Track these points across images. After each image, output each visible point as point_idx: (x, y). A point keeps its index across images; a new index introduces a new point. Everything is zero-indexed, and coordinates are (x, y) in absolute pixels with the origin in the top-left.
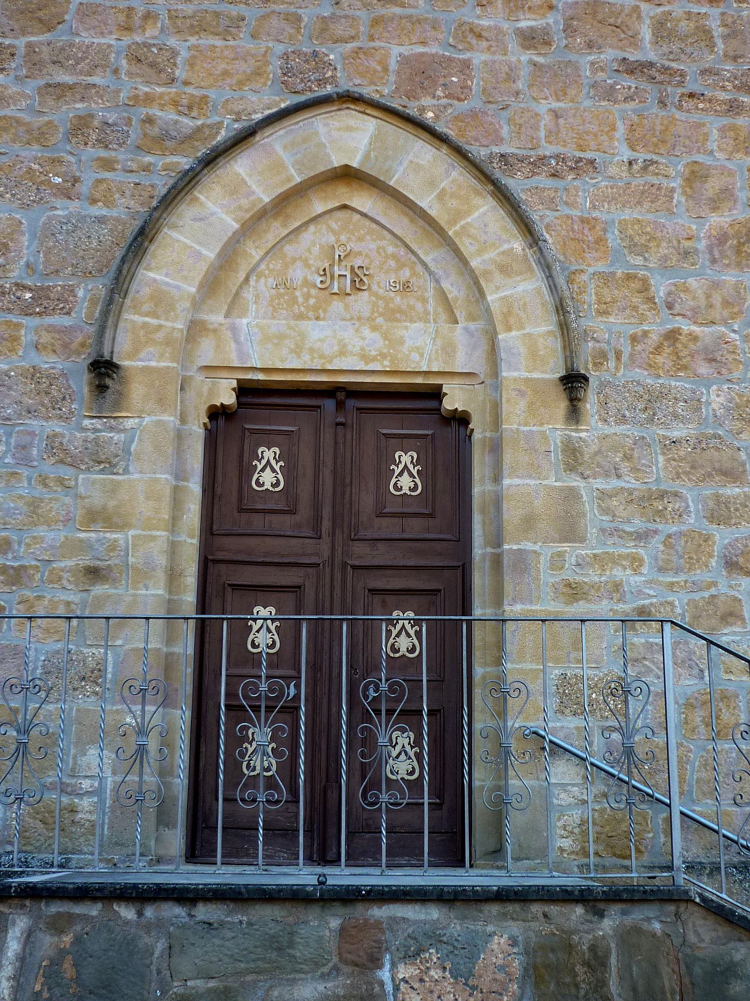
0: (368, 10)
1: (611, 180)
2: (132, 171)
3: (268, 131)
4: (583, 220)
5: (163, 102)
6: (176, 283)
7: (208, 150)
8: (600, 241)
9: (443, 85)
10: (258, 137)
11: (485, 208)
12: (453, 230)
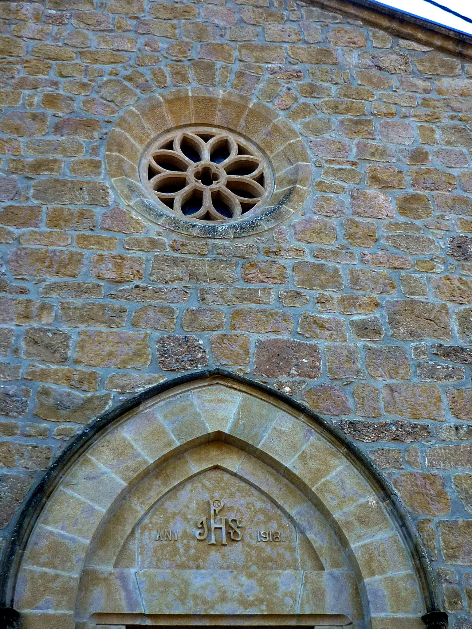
0: (229, 305)
1: (443, 442)
2: (30, 436)
3: (150, 403)
4: (424, 477)
5: (57, 377)
6: (71, 535)
7: (98, 418)
8: (440, 494)
9: (296, 365)
10: (141, 408)
11: (341, 467)
12: (315, 486)
